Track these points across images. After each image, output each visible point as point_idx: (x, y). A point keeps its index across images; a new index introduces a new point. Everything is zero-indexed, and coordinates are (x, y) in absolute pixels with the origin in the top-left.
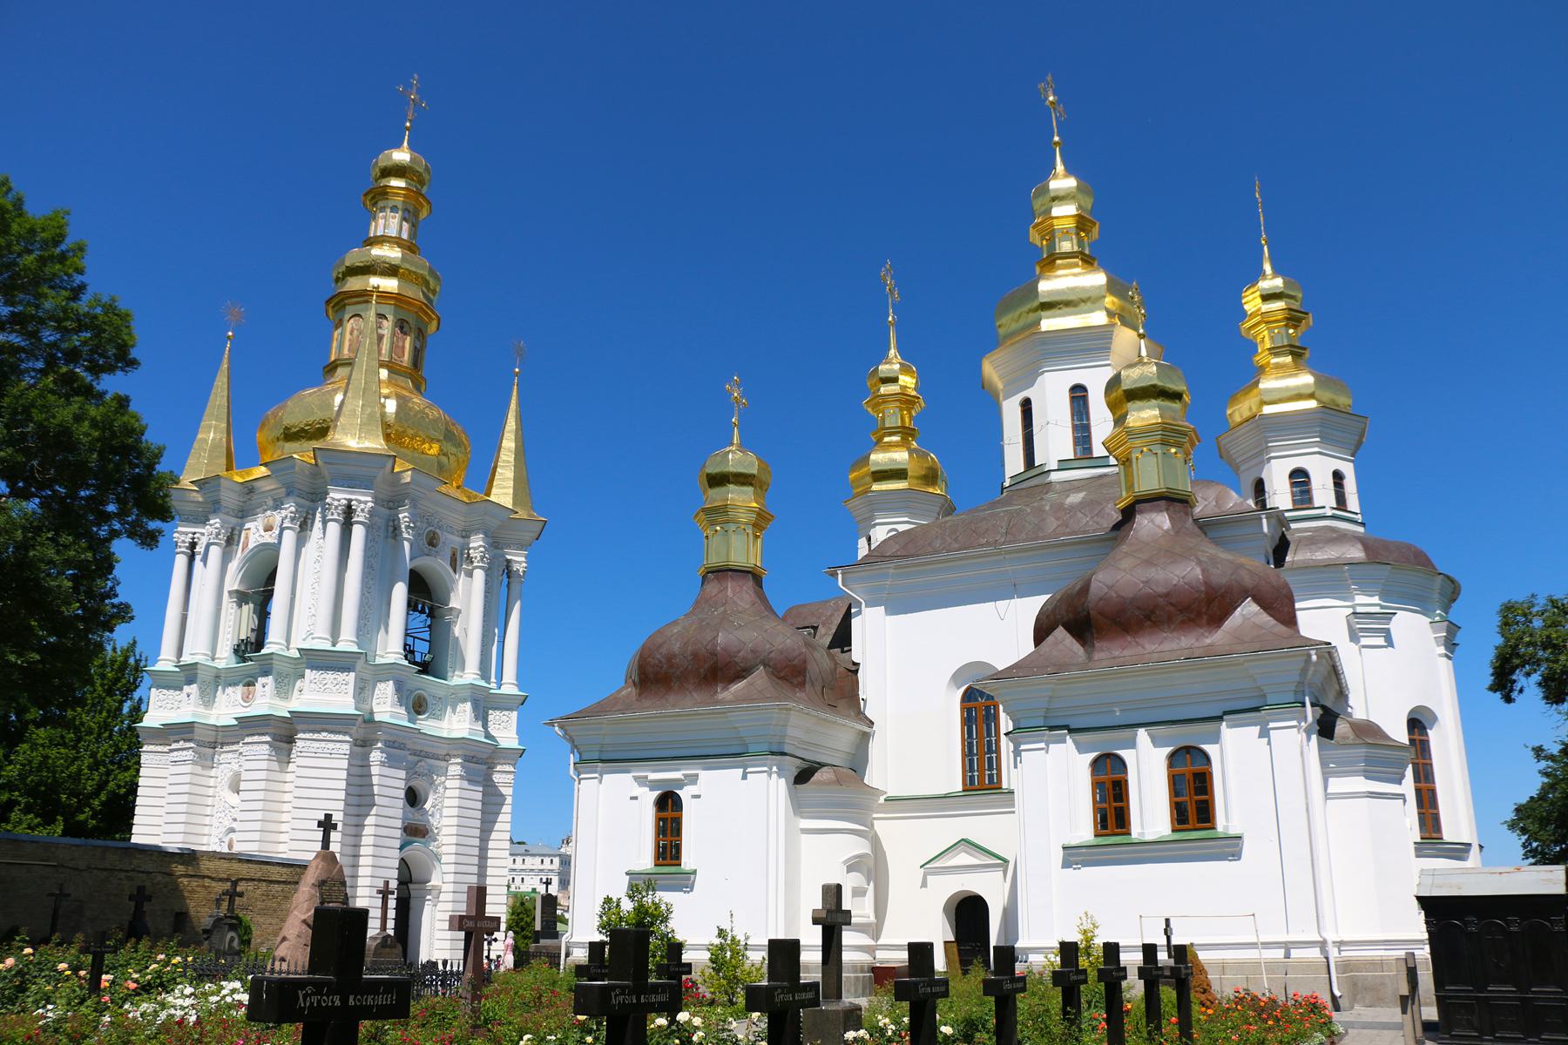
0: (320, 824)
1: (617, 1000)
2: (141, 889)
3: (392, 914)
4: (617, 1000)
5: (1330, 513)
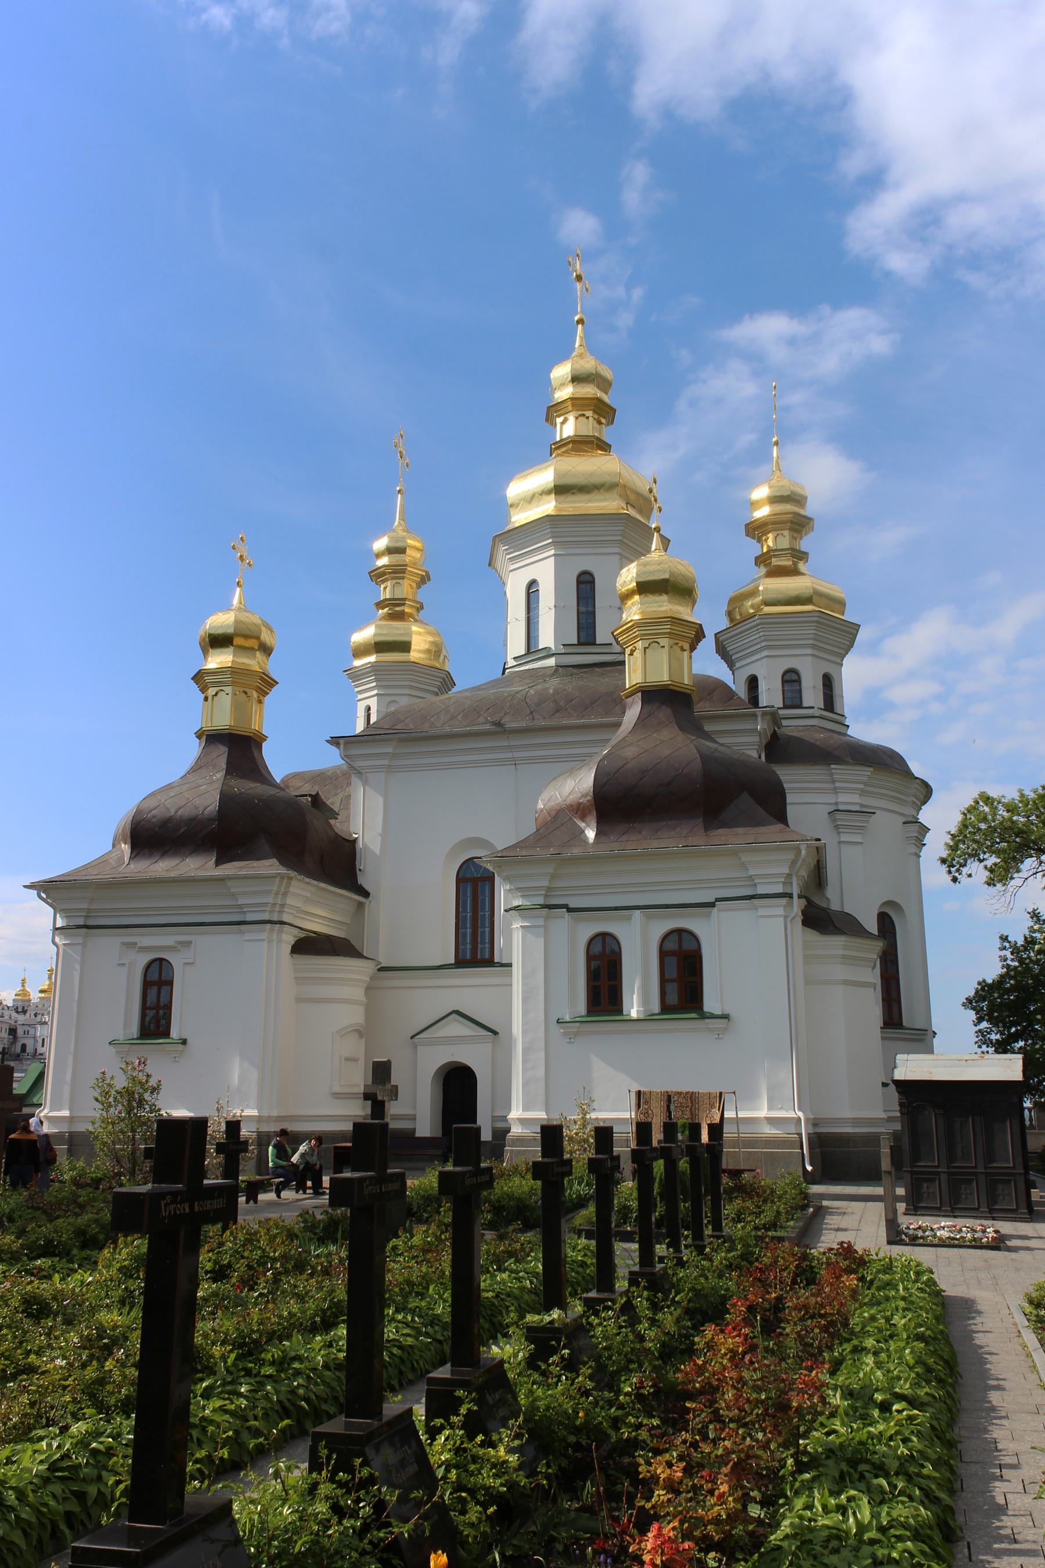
5: (817, 713)
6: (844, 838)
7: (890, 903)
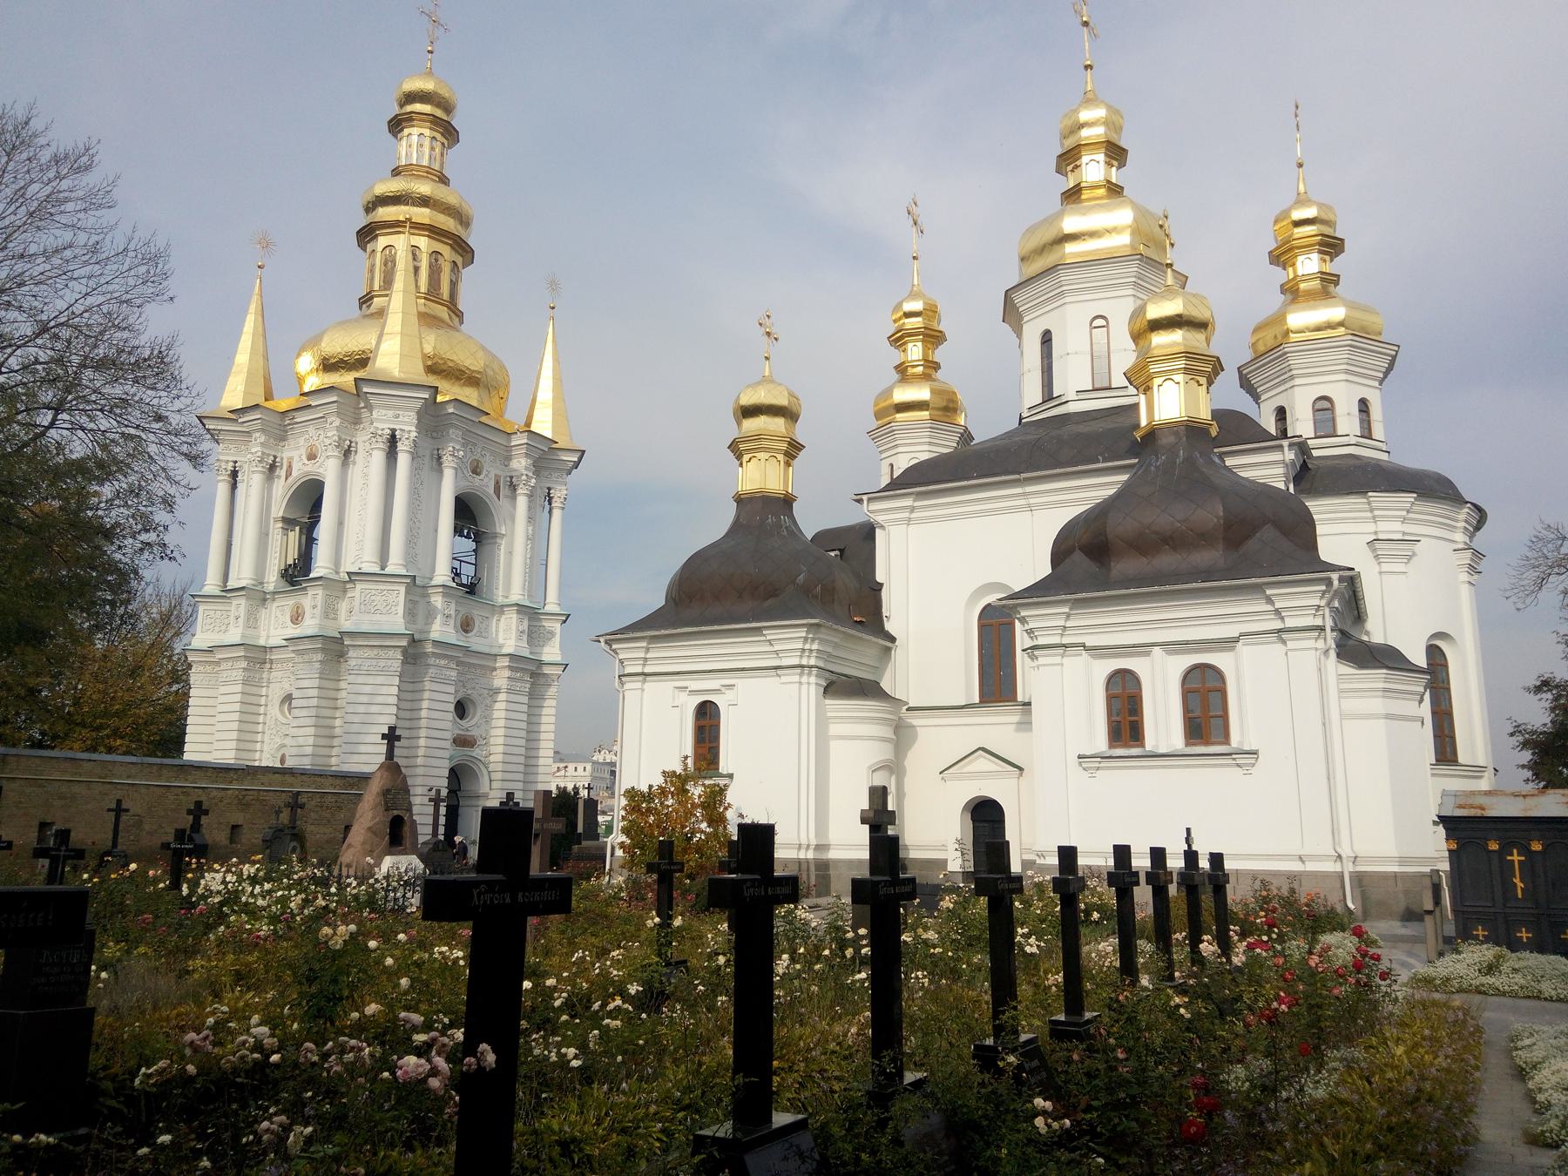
0: (384, 736)
1: (748, 892)
2: (199, 804)
3: (442, 820)
4: (748, 892)
5: (1353, 440)
6: (1385, 567)
7: (1441, 635)
